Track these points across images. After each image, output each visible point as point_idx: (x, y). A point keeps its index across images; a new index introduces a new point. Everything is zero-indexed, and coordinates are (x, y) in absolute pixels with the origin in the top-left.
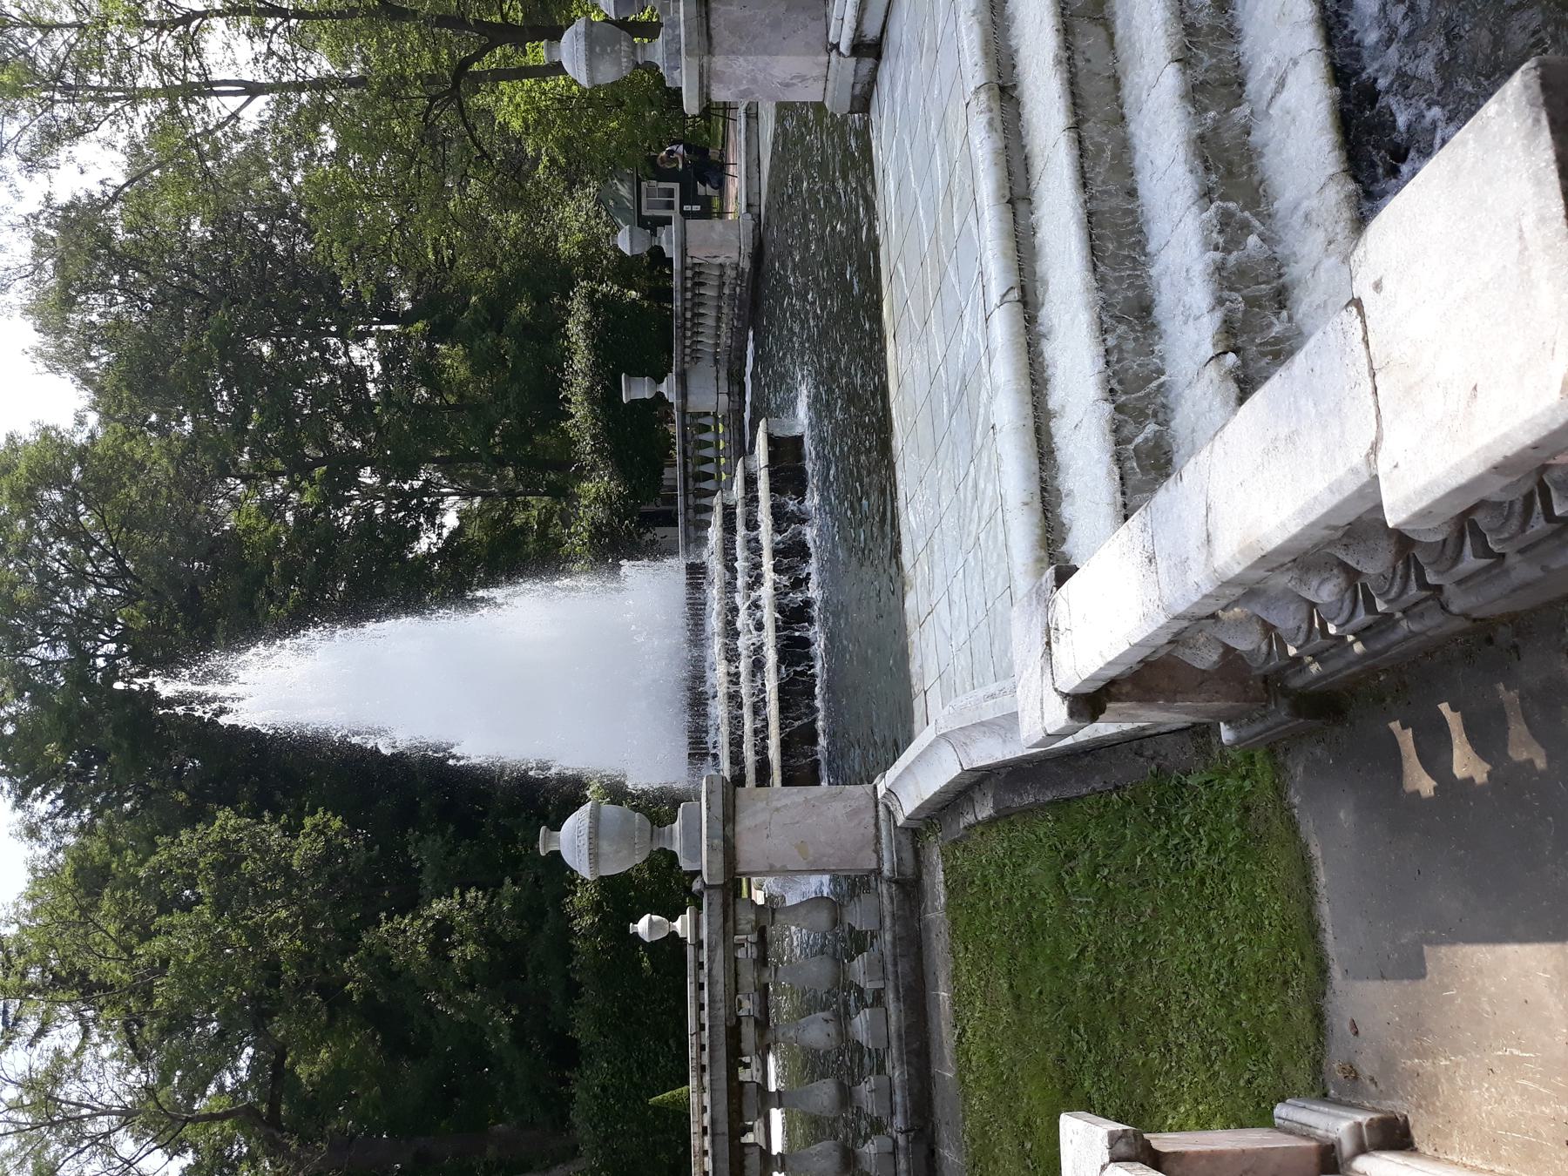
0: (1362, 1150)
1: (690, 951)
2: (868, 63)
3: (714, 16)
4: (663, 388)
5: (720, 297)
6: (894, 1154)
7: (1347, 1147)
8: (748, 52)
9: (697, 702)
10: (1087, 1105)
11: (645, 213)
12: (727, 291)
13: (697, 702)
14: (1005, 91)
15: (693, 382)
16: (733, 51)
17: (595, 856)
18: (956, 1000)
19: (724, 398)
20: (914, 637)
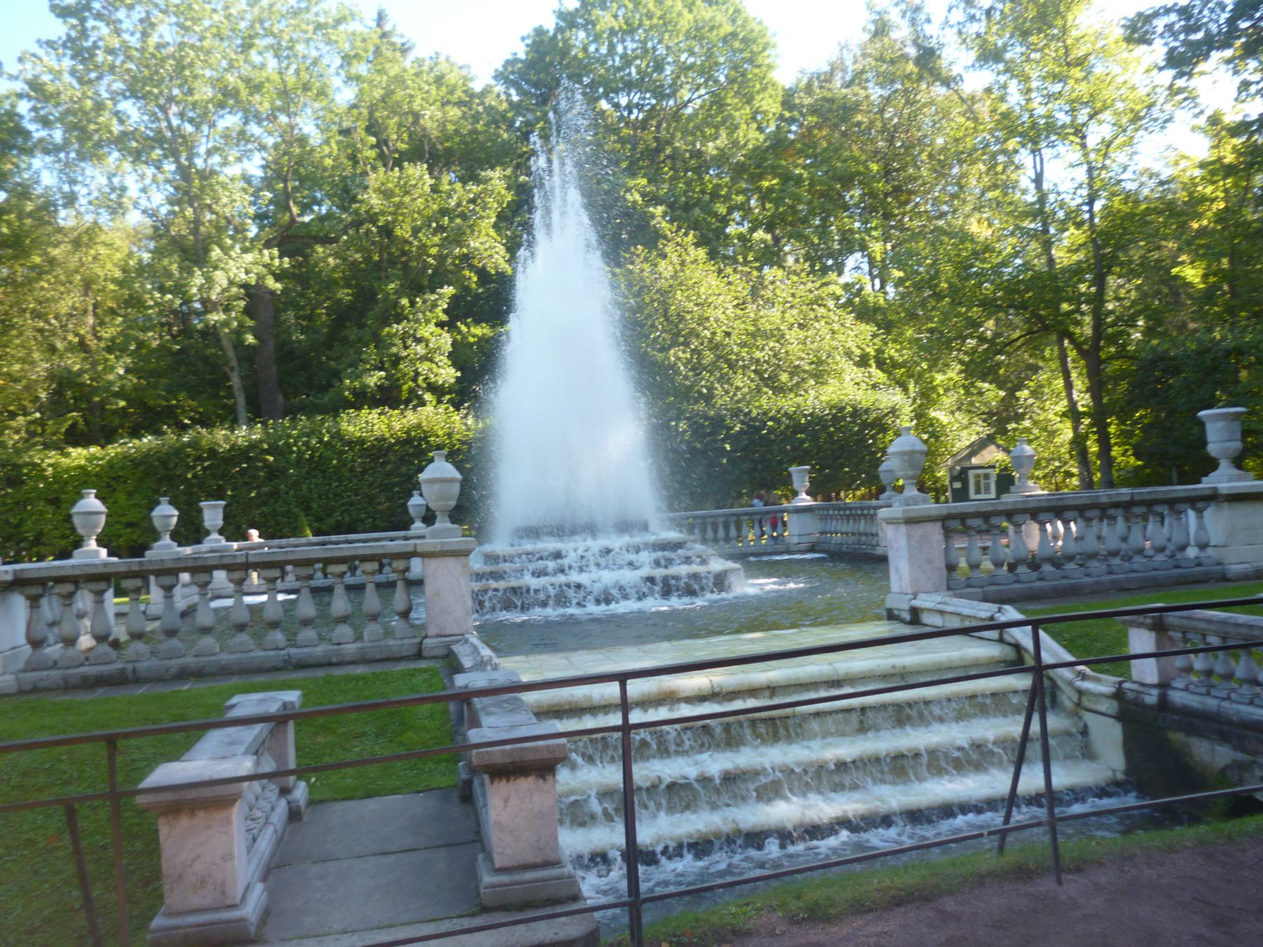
0: (289, 803)
1: (402, 533)
2: (907, 617)
3: (931, 524)
4: (1225, 468)
5: (860, 534)
6: (277, 649)
7: (290, 797)
8: (909, 546)
9: (561, 530)
10: (304, 696)
11: (971, 473)
12: (863, 538)
13: (561, 530)
14: (365, 541)
15: (807, 518)
16: (909, 537)
17: (431, 481)
18: (356, 678)
19: (795, 540)
20: (562, 655)
